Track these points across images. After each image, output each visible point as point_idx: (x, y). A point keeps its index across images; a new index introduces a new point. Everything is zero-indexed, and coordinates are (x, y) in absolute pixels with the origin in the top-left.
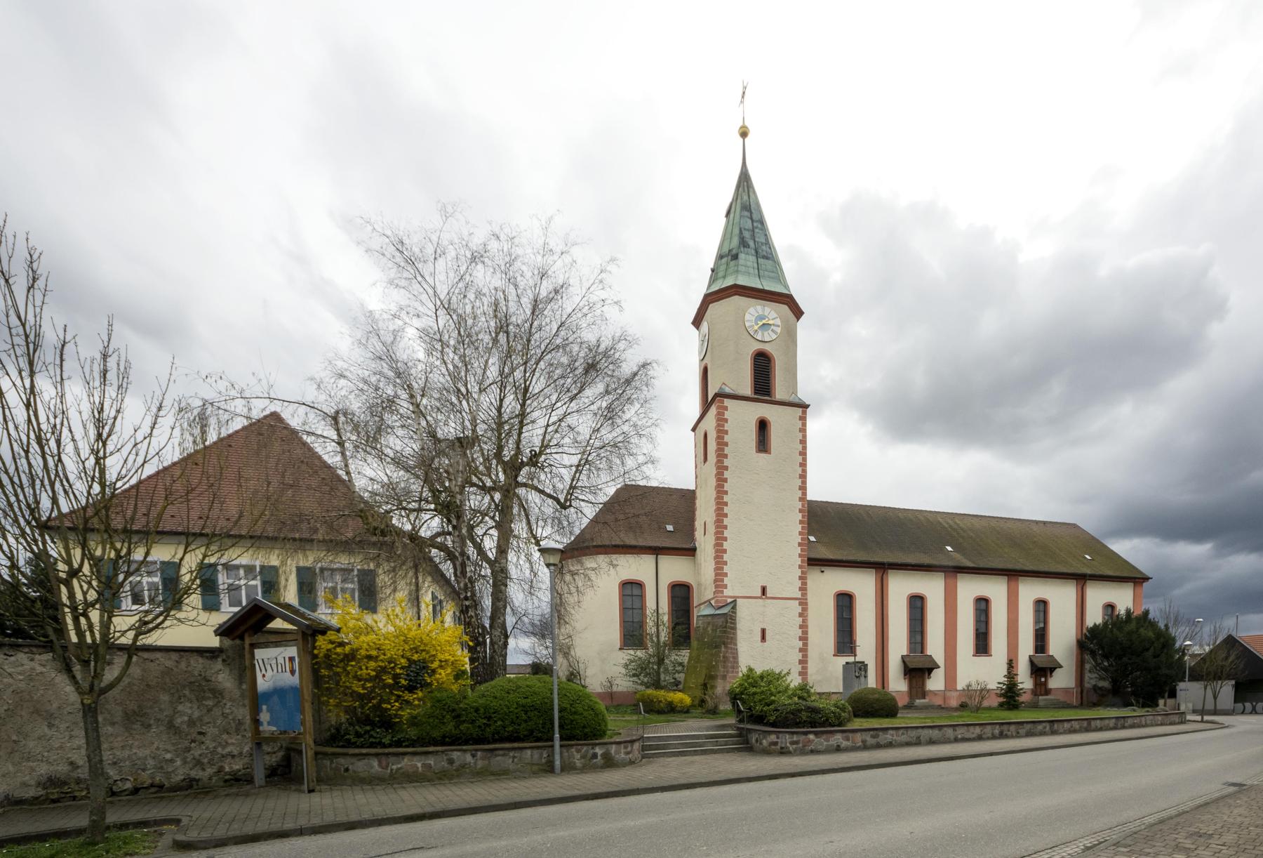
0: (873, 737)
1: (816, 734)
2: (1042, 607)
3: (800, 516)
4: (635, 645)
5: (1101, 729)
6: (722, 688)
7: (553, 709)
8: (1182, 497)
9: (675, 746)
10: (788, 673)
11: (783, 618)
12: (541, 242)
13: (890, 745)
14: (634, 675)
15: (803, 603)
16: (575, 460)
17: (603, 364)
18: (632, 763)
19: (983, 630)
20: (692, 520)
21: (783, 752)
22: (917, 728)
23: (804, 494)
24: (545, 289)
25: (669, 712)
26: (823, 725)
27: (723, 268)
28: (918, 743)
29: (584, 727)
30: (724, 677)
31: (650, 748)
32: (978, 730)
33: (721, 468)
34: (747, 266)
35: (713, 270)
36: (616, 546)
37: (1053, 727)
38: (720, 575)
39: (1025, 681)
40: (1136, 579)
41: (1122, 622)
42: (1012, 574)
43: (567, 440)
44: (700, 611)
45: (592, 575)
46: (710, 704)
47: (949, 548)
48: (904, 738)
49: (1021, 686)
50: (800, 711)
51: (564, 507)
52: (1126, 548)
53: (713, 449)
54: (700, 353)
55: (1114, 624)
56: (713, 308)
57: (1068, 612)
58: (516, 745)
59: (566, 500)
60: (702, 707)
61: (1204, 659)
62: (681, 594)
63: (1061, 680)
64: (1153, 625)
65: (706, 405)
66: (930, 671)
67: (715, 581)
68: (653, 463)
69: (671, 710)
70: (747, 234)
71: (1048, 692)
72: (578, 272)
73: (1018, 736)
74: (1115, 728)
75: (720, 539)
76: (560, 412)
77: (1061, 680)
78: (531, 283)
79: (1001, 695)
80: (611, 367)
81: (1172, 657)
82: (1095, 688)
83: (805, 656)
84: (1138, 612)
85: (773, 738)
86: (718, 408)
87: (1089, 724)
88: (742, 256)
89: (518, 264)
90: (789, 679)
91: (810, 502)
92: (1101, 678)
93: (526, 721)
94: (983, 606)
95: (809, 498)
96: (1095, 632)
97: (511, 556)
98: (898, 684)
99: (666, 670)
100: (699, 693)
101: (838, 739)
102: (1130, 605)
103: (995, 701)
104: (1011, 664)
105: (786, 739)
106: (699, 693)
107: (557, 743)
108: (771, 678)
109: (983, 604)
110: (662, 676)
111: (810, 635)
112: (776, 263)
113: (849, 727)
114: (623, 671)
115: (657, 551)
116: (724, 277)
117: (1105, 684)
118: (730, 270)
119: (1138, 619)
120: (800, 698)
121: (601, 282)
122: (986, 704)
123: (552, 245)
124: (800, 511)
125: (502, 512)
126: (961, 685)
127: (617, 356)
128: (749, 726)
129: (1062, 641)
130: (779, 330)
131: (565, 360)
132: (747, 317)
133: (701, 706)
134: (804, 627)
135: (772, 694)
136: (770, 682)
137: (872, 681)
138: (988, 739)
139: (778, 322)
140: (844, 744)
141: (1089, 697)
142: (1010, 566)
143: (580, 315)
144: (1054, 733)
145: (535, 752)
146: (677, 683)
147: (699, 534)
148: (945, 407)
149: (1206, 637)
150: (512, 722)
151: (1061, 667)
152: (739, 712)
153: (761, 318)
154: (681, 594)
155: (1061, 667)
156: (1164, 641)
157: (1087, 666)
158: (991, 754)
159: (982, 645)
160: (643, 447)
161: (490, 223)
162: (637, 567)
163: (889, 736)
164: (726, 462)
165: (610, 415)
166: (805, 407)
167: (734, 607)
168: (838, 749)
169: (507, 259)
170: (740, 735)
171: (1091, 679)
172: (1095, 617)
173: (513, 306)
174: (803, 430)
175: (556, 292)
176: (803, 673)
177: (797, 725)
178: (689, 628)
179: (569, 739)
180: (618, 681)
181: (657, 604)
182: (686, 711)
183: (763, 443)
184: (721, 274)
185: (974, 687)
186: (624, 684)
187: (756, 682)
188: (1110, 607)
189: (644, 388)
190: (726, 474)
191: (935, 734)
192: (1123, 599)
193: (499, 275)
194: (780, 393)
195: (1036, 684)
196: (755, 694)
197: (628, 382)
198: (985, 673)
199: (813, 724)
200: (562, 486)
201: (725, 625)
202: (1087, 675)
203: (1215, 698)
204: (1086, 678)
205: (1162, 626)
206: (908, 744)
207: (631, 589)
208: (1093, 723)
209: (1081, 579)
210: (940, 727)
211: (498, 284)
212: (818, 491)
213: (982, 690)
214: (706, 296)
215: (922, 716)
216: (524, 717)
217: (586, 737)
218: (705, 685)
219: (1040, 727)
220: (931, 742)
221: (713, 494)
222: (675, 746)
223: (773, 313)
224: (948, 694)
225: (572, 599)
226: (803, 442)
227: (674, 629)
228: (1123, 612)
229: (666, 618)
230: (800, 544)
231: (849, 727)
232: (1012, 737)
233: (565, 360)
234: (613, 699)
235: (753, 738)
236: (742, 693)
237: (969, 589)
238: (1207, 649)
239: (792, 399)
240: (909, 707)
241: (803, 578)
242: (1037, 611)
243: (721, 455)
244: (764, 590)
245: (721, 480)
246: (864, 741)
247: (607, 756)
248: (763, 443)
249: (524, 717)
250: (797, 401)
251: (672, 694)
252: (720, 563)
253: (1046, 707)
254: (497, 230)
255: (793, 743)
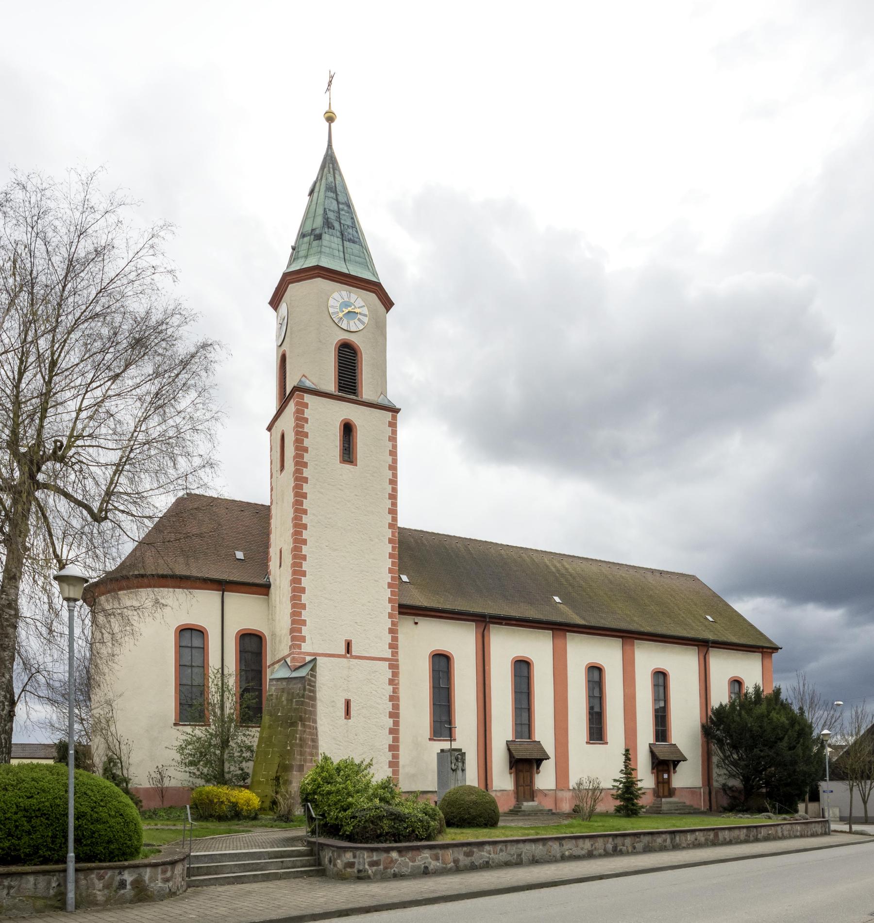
0: (468, 854)
1: (400, 851)
2: (661, 678)
3: (389, 548)
4: (193, 719)
5: (730, 843)
6: (298, 781)
7: (66, 815)
8: (805, 552)
9: (231, 869)
10: (370, 765)
11: (367, 684)
12: (80, 197)
13: (487, 866)
14: (191, 763)
15: (394, 666)
16: (114, 457)
17: (153, 340)
18: (172, 894)
19: (597, 709)
20: (266, 545)
21: (361, 877)
22: (518, 842)
23: (395, 519)
24: (84, 248)
25: (232, 818)
26: (408, 838)
27: (305, 247)
28: (518, 863)
29: (109, 842)
30: (301, 768)
31: (199, 871)
32: (587, 845)
33: (300, 480)
34: (329, 250)
35: (294, 249)
36: (164, 577)
37: (674, 840)
38: (297, 622)
39: (646, 780)
40: (764, 649)
41: (750, 702)
42: (629, 636)
43: (103, 430)
44: (275, 673)
45: (134, 617)
46: (283, 808)
47: (557, 599)
48: (503, 857)
49: (640, 785)
50: (381, 818)
51: (98, 518)
52: (756, 610)
53: (291, 455)
54: (278, 337)
55: (742, 705)
56: (294, 290)
57: (696, 686)
58: (13, 869)
59: (101, 510)
60: (274, 811)
61: (849, 752)
62: (252, 645)
63: (687, 777)
64: (785, 707)
65: (284, 400)
66: (539, 762)
67: (292, 631)
68: (212, 466)
69: (236, 815)
70: (332, 216)
71: (671, 792)
72: (125, 237)
73: (634, 852)
74: (746, 841)
75: (298, 573)
76: (98, 393)
77: (687, 777)
78: (66, 239)
79: (617, 797)
80: (164, 344)
81: (811, 750)
82: (725, 788)
83: (396, 740)
84: (768, 691)
85: (348, 856)
86: (297, 404)
87: (716, 835)
88: (326, 237)
89: (49, 218)
90: (372, 771)
91: (402, 531)
92: (731, 776)
93: (29, 833)
94: (596, 674)
95: (401, 524)
96: (720, 712)
97: (25, 585)
98: (503, 781)
99: (232, 757)
100: (270, 791)
101: (425, 858)
102: (760, 682)
103: (610, 805)
104: (628, 756)
105: (364, 859)
106: (270, 791)
107: (71, 865)
108: (350, 770)
109: (596, 673)
110: (227, 765)
111: (402, 711)
112: (364, 248)
113: (441, 840)
114: (178, 757)
115: (223, 586)
116: (306, 257)
117: (736, 783)
118: (312, 251)
119: (769, 699)
120: (381, 800)
121: (152, 247)
122: (600, 808)
123: (94, 201)
124: (391, 541)
125: (14, 525)
126: (572, 783)
127: (169, 332)
128: (322, 840)
129: (686, 728)
130: (366, 320)
131: (105, 331)
132: (331, 302)
133: (271, 809)
134: (394, 698)
135: (349, 795)
136: (347, 777)
137: (471, 777)
138: (600, 856)
139: (365, 311)
140: (434, 864)
141: (740, 802)
142: (623, 626)
143: (125, 281)
144: (676, 847)
145: (41, 879)
146: (244, 776)
147: (273, 565)
148: (544, 425)
149: (846, 724)
150: (10, 834)
151: (685, 760)
152: (311, 819)
153: (346, 304)
154: (252, 645)
155: (685, 760)
156: (799, 729)
157: (715, 759)
158: (601, 877)
159: (597, 732)
160: (200, 446)
161: (15, 171)
162: (198, 607)
163: (484, 854)
164: (306, 473)
165: (159, 403)
166: (396, 411)
167: (313, 669)
168: (426, 872)
169: (35, 211)
170: (310, 853)
171: (720, 778)
172: (720, 696)
173: (40, 263)
174: (393, 439)
175: (97, 253)
176: (394, 764)
177: (378, 838)
178: (260, 697)
179: (90, 858)
180: (171, 772)
181: (222, 660)
182: (253, 817)
183: (348, 454)
184: (302, 253)
185: (586, 785)
186: (178, 777)
187: (331, 776)
188: (737, 683)
189: (203, 373)
190: (306, 488)
191: (538, 850)
192: (751, 672)
193: (23, 228)
194: (367, 392)
195: (658, 783)
196: (329, 793)
197: (185, 364)
198: (596, 767)
199: (397, 837)
200: (95, 493)
201: (302, 690)
202: (715, 771)
203: (865, 802)
204: (715, 775)
205: (796, 710)
206: (507, 864)
207: (190, 637)
208: (721, 835)
209: (704, 646)
210: (544, 841)
211: (25, 238)
212: (414, 516)
213: (594, 790)
214: (285, 275)
215: (527, 824)
216: (27, 827)
217: (111, 857)
218: (277, 779)
219: (659, 840)
220: (535, 861)
221: (290, 513)
222: (231, 869)
223: (360, 300)
224: (560, 794)
225: (104, 651)
226: (393, 453)
227: (242, 695)
228: (751, 690)
229: (231, 682)
230: (390, 585)
231: (441, 840)
232: (628, 853)
233: (105, 331)
234: (164, 802)
235: (327, 855)
236: (315, 793)
237: (582, 652)
238: (851, 740)
239: (381, 400)
240: (515, 812)
241: (393, 631)
242: (656, 686)
243: (300, 464)
244: (348, 645)
245: (300, 496)
246: (456, 861)
247: (138, 885)
248: (348, 454)
249: (27, 827)
250: (386, 403)
251: (236, 792)
252: (297, 606)
253: (670, 813)
254: (23, 180)
255: (373, 864)
